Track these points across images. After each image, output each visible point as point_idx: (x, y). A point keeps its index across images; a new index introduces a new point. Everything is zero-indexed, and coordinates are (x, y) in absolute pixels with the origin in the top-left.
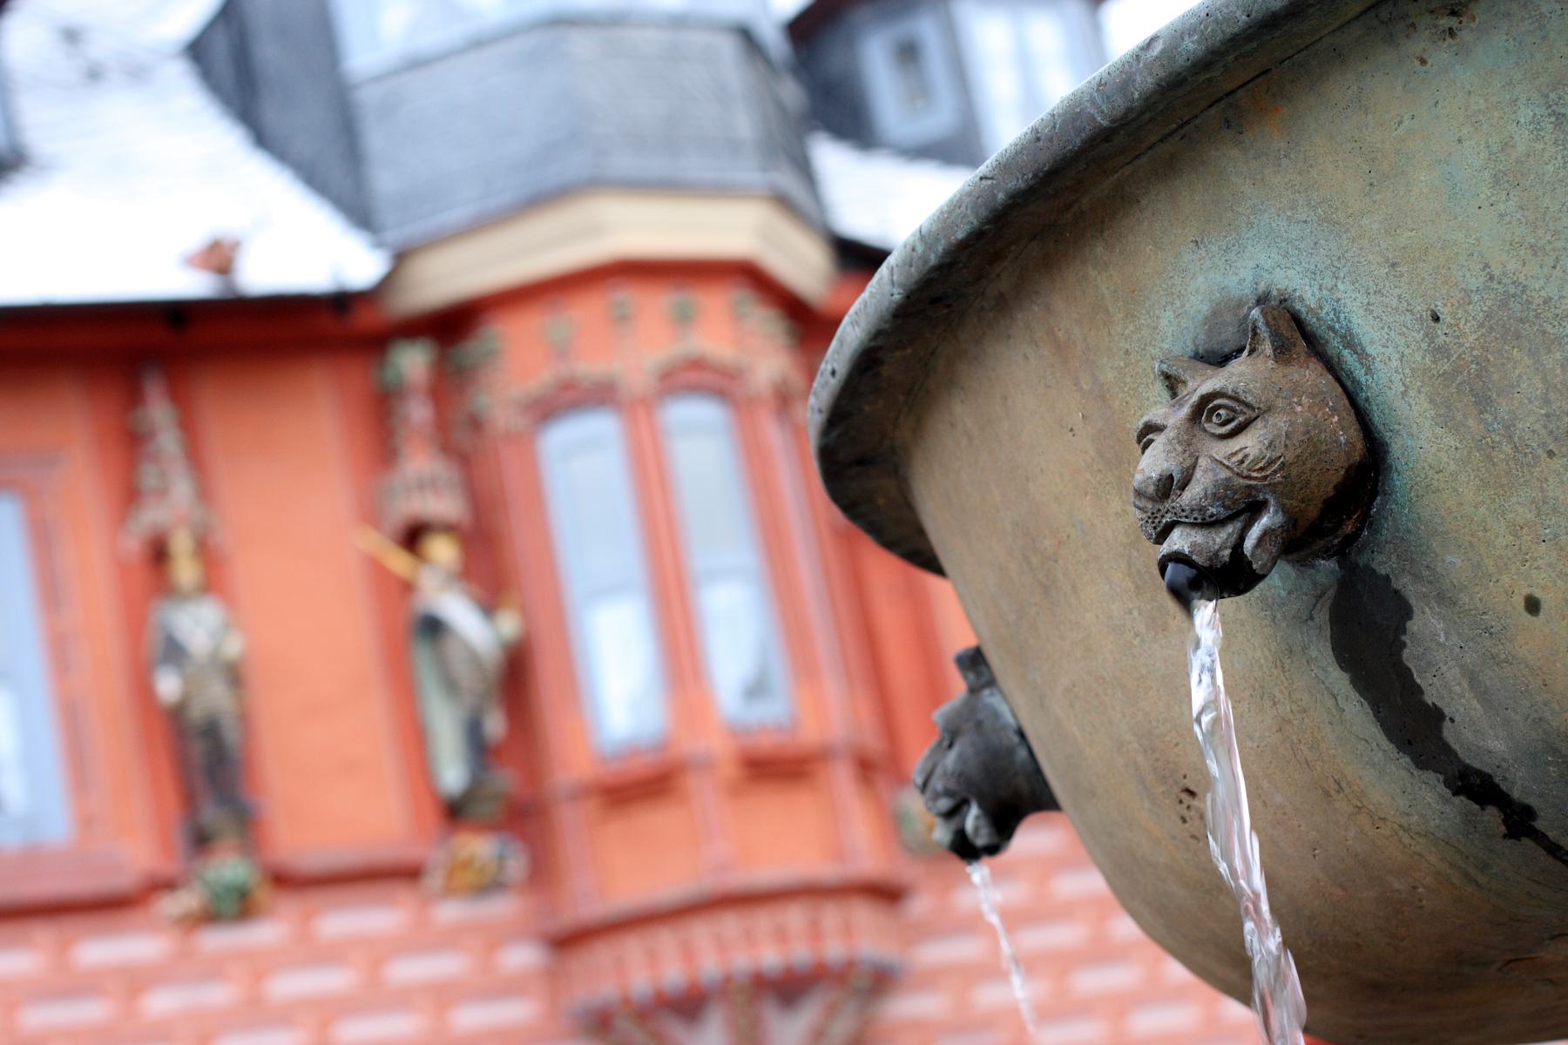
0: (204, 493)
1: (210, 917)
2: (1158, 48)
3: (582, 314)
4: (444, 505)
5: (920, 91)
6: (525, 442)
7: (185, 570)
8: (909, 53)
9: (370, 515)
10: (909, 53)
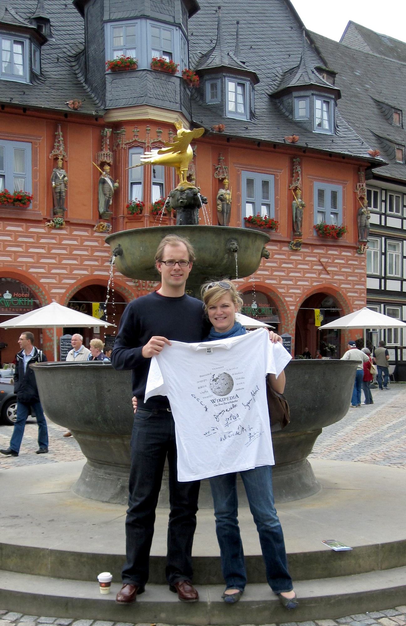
0: (65, 150)
1: (54, 228)
2: (115, 502)
3: (141, 129)
4: (110, 160)
5: (214, 96)
6: (126, 151)
7: (60, 163)
8: (214, 86)
9: (95, 160)
10: (214, 86)
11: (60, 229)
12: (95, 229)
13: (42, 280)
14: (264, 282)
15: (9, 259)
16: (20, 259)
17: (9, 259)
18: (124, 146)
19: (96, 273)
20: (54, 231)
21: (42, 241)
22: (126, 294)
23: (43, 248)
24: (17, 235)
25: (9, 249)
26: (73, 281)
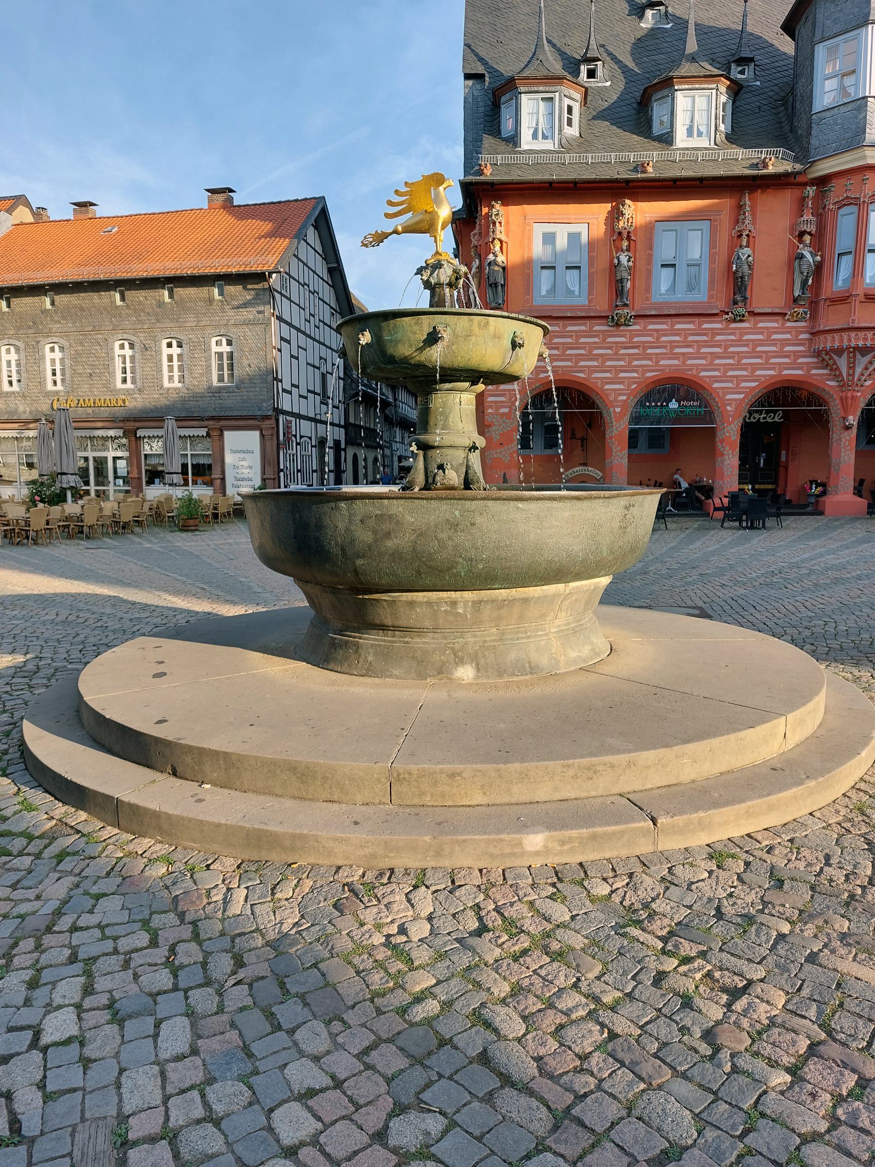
1: (735, 321)
11: (741, 321)
12: (786, 318)
13: (715, 385)
14: (780, 375)
15: (676, 362)
16: (689, 362)
17: (676, 362)
18: (831, 206)
19: (785, 372)
20: (733, 325)
21: (718, 338)
22: (826, 397)
23: (719, 346)
24: (579, 334)
25: (676, 350)
26: (754, 384)
